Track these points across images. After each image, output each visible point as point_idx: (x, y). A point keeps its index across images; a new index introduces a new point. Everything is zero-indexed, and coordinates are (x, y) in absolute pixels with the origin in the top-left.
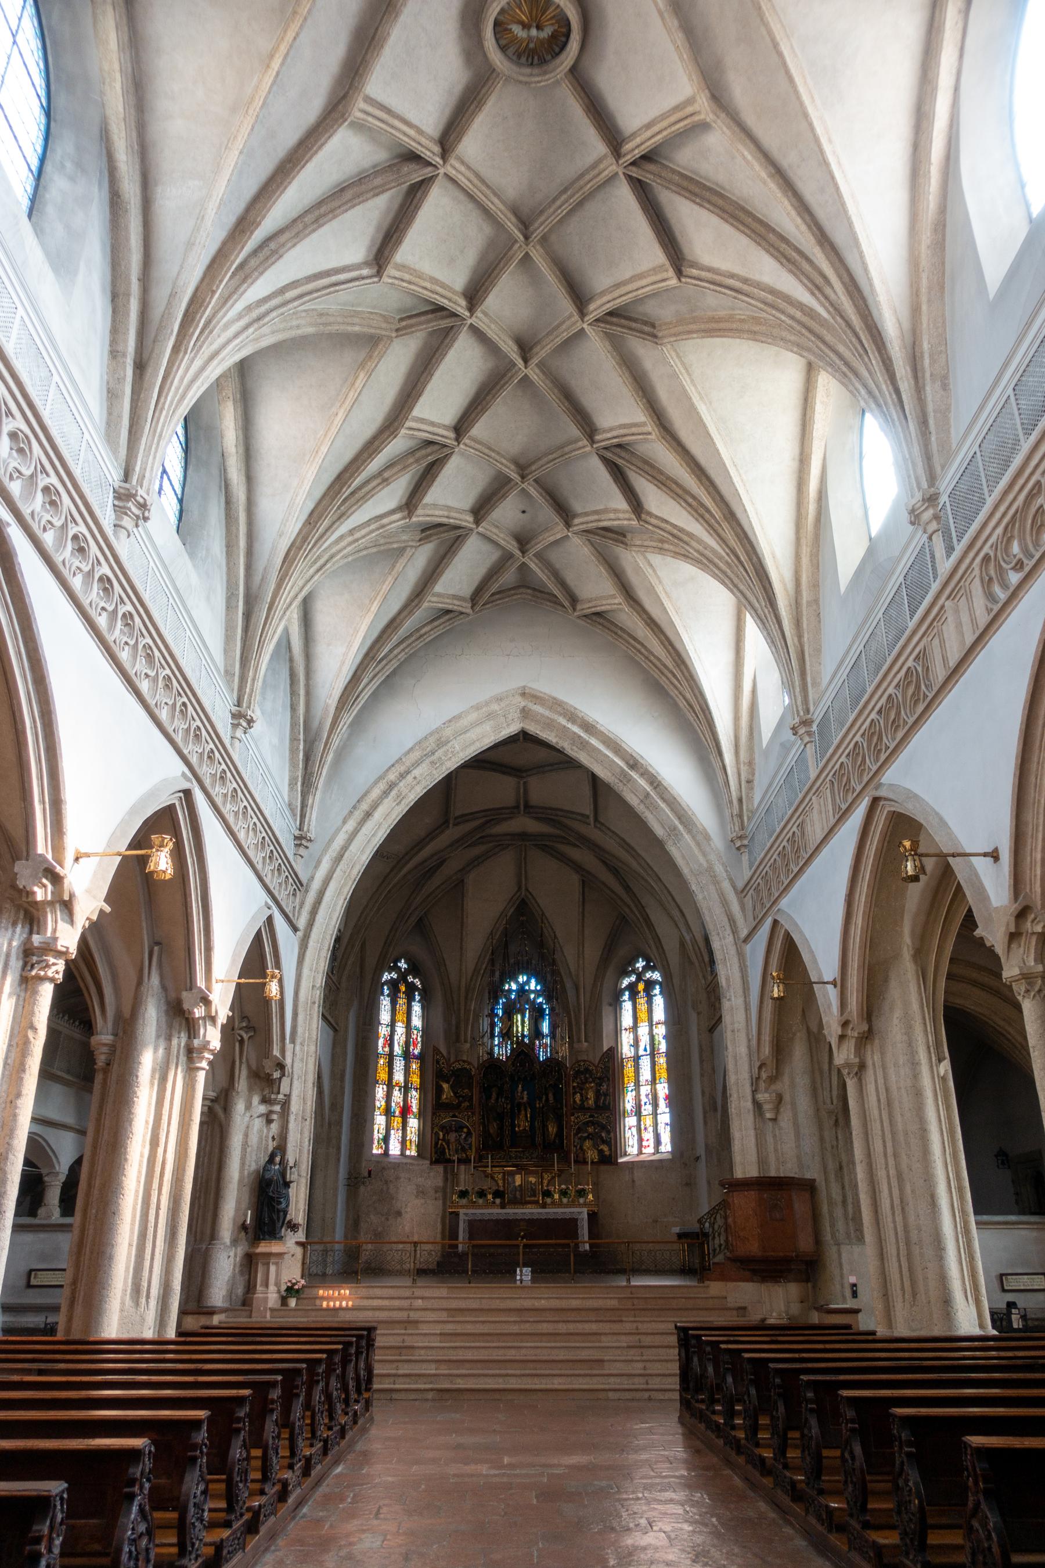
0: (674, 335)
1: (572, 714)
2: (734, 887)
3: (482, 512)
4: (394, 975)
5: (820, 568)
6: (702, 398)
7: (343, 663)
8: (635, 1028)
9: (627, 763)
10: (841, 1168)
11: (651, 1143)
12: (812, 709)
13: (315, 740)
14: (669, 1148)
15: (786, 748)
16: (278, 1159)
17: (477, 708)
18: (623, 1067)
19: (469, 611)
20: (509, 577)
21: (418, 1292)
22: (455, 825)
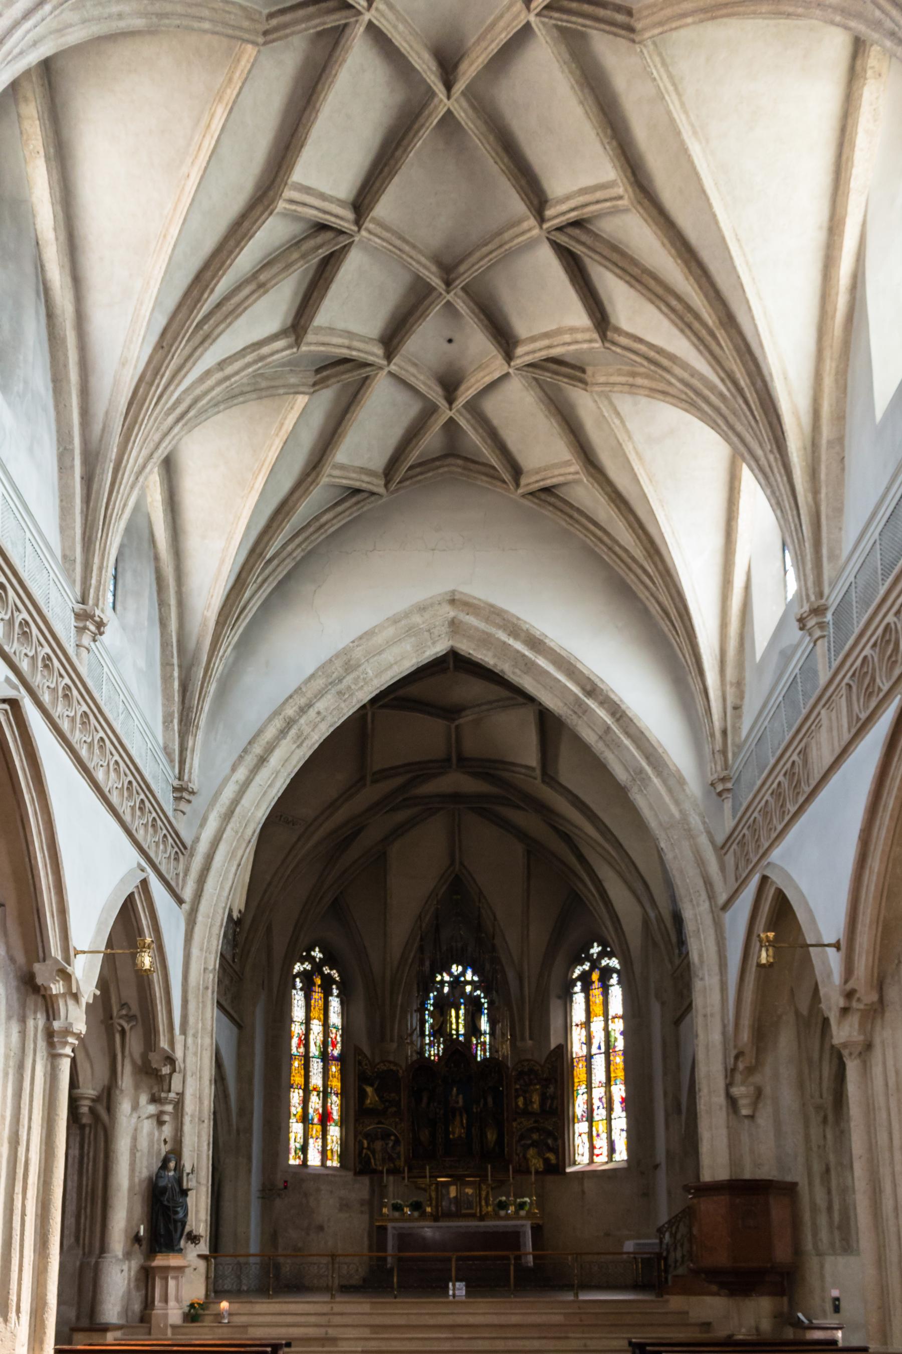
0: (661, 24)
1: (515, 625)
2: (713, 842)
3: (395, 342)
4: (308, 966)
5: (849, 390)
6: (695, 133)
7: (222, 561)
8: (587, 1024)
9: (583, 689)
10: (828, 1170)
11: (605, 1151)
12: (826, 591)
13: (191, 665)
14: (624, 1156)
15: (786, 656)
16: (172, 1165)
17: (395, 620)
18: (573, 1067)
19: (381, 490)
20: (431, 440)
21: (337, 1308)
22: (375, 781)
